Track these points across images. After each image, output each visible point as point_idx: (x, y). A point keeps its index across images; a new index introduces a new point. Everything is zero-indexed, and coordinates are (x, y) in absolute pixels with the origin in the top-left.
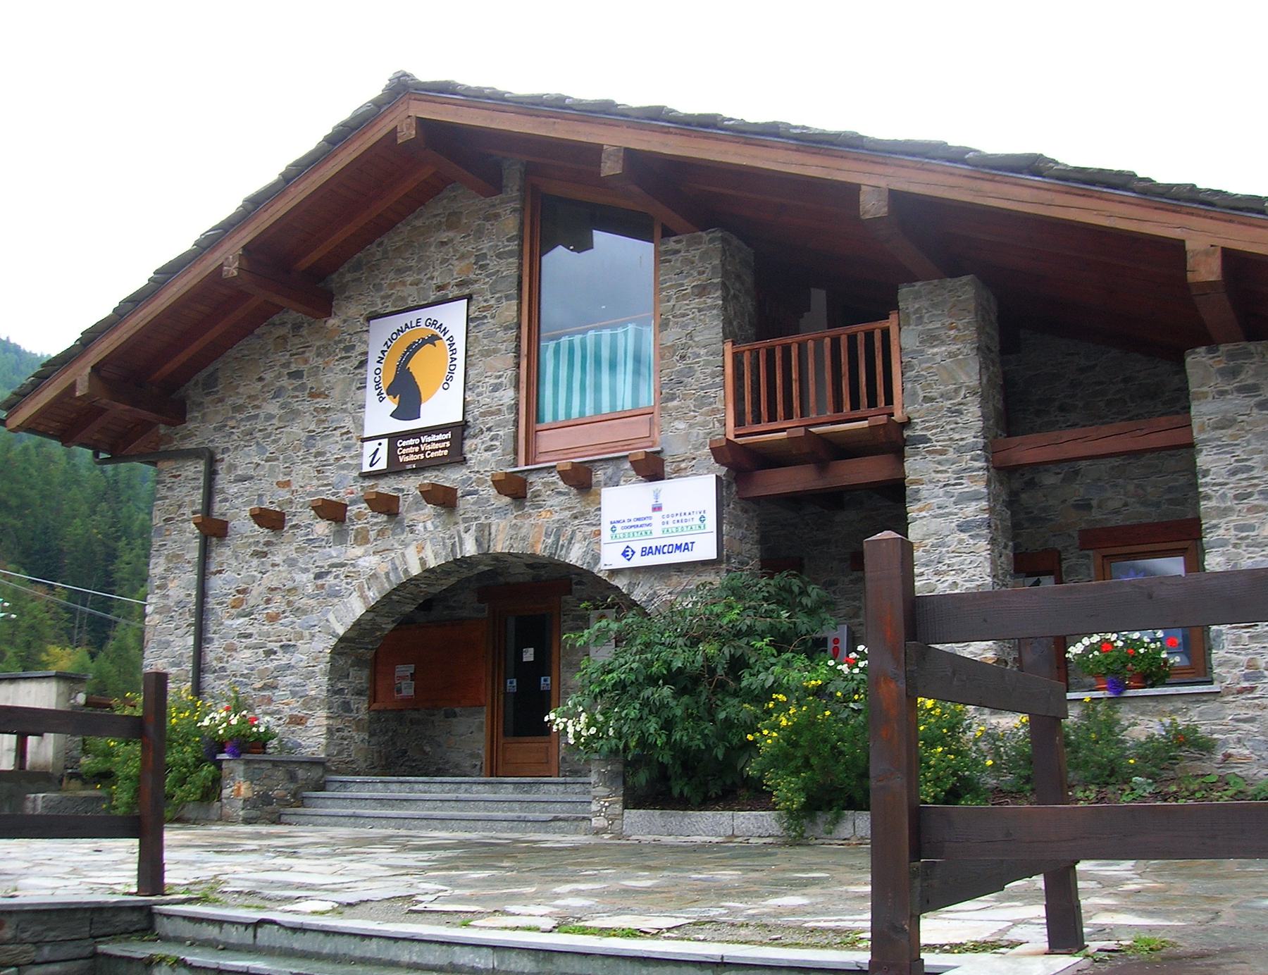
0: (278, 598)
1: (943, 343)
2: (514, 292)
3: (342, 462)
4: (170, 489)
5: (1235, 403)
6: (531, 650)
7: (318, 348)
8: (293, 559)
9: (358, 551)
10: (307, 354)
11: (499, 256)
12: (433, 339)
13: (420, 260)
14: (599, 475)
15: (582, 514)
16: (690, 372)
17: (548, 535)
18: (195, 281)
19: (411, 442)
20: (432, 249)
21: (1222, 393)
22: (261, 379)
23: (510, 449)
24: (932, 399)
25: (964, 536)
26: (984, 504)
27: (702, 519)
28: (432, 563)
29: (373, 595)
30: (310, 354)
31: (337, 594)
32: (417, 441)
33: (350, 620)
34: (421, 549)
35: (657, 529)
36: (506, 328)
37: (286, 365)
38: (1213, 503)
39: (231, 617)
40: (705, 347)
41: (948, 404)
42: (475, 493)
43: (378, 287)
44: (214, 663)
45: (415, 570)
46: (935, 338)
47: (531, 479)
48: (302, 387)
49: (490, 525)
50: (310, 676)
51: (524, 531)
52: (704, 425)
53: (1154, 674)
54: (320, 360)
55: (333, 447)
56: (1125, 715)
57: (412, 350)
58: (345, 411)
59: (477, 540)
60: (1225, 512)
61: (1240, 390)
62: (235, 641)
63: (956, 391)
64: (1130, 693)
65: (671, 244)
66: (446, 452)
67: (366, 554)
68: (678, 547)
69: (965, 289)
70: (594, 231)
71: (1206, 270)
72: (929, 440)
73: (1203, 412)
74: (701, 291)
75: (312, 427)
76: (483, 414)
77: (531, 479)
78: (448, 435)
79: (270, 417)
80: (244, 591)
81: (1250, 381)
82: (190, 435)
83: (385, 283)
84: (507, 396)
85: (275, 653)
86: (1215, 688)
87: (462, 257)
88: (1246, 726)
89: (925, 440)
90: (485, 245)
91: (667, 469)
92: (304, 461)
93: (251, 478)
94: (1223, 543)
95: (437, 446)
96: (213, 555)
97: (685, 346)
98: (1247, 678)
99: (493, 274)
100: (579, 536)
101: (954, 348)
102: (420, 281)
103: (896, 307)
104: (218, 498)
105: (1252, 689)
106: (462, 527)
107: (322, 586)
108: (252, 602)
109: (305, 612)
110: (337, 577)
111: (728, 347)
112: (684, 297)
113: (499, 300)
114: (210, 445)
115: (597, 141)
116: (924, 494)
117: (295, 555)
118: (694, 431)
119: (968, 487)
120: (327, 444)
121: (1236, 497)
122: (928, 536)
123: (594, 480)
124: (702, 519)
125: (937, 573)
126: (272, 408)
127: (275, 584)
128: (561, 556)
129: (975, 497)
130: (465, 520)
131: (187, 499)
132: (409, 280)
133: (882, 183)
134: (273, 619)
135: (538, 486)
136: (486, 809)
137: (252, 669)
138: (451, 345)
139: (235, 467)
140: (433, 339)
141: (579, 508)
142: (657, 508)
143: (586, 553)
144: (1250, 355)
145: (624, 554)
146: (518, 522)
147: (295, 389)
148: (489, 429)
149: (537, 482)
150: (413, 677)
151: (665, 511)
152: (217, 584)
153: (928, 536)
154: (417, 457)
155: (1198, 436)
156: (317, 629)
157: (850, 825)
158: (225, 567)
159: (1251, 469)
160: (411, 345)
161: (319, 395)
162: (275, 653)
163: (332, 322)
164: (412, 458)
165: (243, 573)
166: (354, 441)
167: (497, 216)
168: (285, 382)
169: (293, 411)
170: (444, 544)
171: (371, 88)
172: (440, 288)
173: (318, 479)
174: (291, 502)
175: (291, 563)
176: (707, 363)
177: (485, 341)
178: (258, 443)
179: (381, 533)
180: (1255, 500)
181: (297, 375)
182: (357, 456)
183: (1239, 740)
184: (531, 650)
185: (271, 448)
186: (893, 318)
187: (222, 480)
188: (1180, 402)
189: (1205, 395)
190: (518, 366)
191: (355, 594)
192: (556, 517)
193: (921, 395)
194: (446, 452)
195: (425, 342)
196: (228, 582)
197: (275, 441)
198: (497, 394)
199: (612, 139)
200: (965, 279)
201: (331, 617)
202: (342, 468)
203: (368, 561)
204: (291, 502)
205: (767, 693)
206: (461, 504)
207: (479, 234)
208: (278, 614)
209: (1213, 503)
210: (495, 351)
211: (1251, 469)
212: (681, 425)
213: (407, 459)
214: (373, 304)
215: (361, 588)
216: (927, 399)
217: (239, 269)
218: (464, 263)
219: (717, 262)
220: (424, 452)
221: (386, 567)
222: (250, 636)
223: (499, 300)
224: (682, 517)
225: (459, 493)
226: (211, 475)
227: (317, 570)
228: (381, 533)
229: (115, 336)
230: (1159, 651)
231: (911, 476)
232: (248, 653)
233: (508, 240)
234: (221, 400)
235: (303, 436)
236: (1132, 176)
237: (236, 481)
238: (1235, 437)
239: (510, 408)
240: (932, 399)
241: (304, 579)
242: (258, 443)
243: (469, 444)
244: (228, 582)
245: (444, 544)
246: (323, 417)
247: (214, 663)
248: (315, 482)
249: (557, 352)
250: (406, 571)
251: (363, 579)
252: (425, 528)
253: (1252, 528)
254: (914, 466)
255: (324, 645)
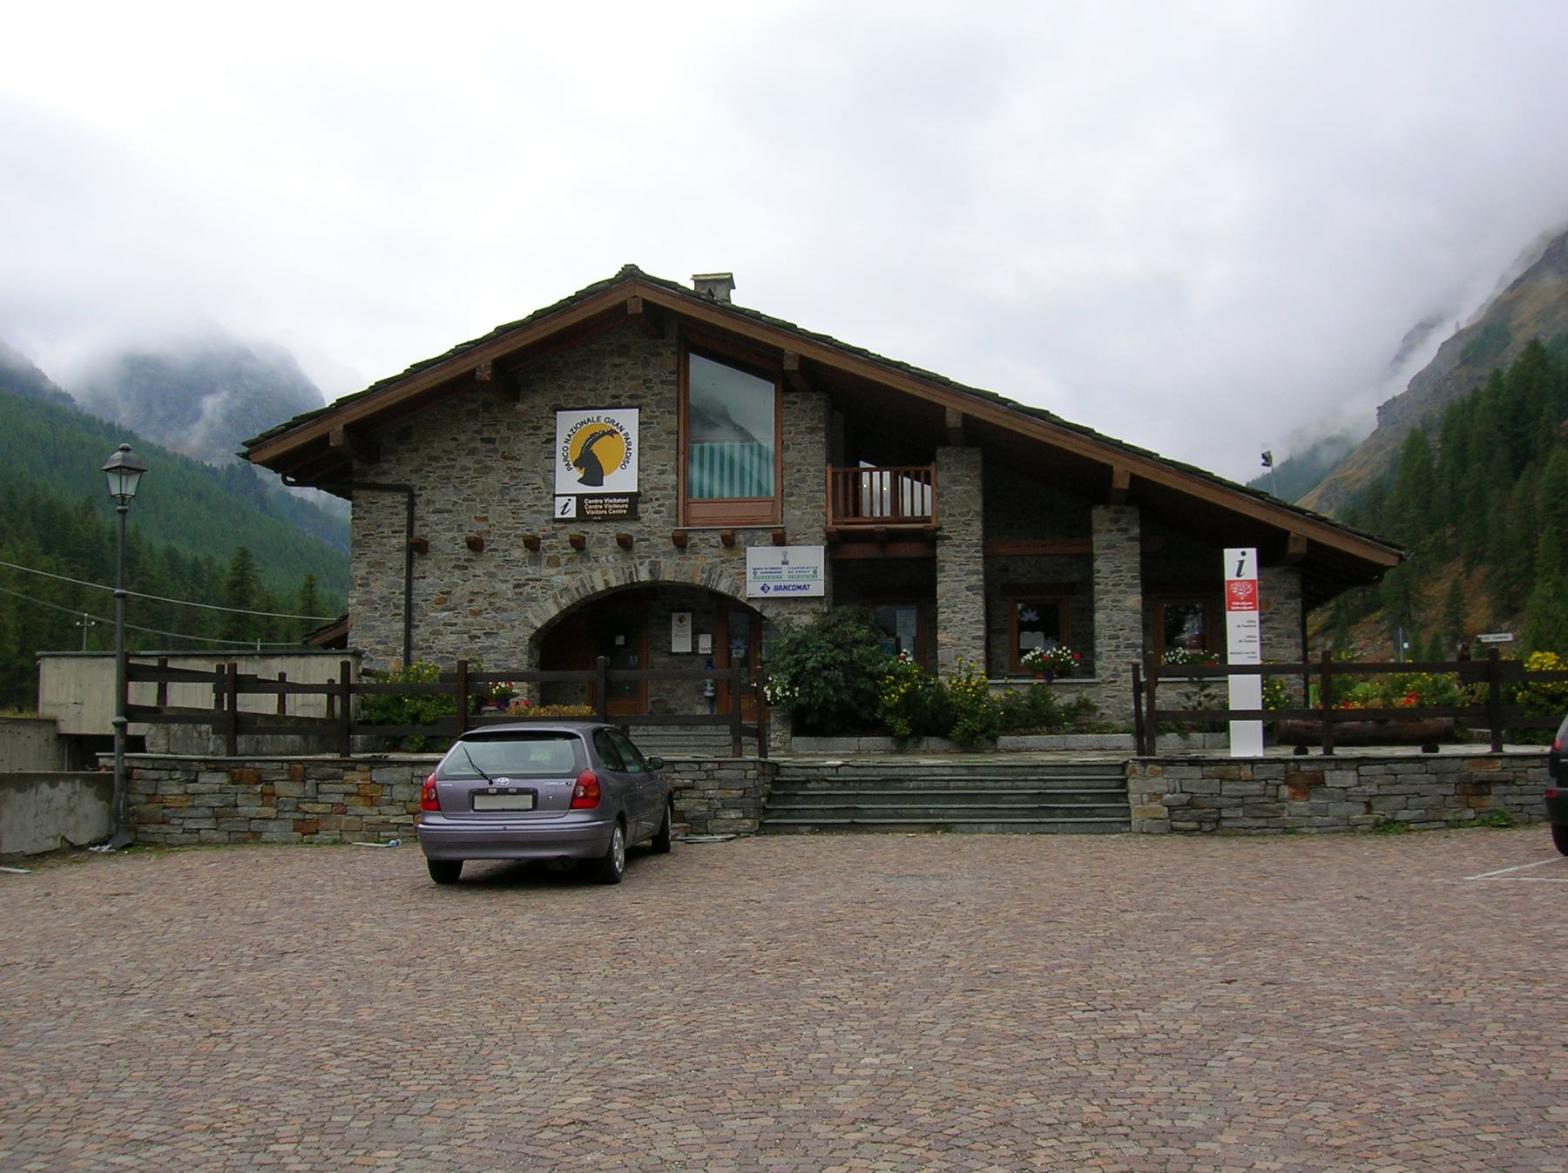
0: (480, 599)
1: (961, 484)
2: (675, 409)
3: (535, 508)
4: (366, 512)
5: (1116, 537)
6: (622, 638)
7: (509, 424)
8: (493, 573)
9: (552, 571)
10: (498, 427)
11: (663, 382)
12: (612, 433)
13: (597, 373)
14: (740, 537)
15: (728, 561)
16: (803, 480)
17: (703, 572)
18: (448, 378)
19: (596, 501)
20: (607, 367)
21: (1110, 531)
22: (455, 439)
23: (674, 514)
24: (954, 516)
25: (969, 593)
26: (981, 577)
27: (815, 572)
28: (614, 584)
29: (565, 602)
30: (502, 427)
31: (534, 600)
32: (601, 501)
33: (547, 618)
34: (604, 574)
35: (785, 575)
36: (669, 433)
37: (479, 432)
38: (1101, 587)
39: (436, 610)
40: (813, 466)
41: (963, 519)
42: (648, 540)
43: (561, 388)
44: (421, 643)
45: (600, 587)
46: (958, 481)
47: (690, 535)
48: (495, 450)
49: (659, 562)
50: (513, 654)
51: (685, 568)
52: (813, 514)
53: (1065, 671)
54: (511, 434)
55: (527, 498)
56: (1051, 690)
57: (595, 437)
58: (536, 472)
59: (650, 572)
60: (1108, 592)
61: (1118, 530)
62: (441, 628)
63: (968, 512)
64: (1055, 681)
65: (791, 397)
66: (625, 511)
67: (559, 573)
68: (799, 587)
69: (976, 456)
70: (691, 355)
71: (1122, 483)
72: (951, 538)
73: (1099, 540)
74: (812, 430)
75: (506, 480)
76: (651, 489)
77: (690, 535)
78: (627, 500)
79: (465, 469)
80: (448, 593)
81: (1124, 526)
82: (385, 473)
83: (567, 386)
84: (671, 479)
85: (479, 638)
86: (1097, 680)
87: (632, 378)
88: (1111, 700)
89: (949, 538)
90: (651, 373)
91: (788, 539)
92: (500, 504)
93: (451, 511)
94: (1105, 608)
95: (621, 506)
96: (416, 564)
97: (800, 464)
98: (1113, 676)
99: (658, 394)
100: (725, 573)
101: (968, 488)
102: (597, 389)
103: (935, 460)
104: (417, 523)
105: (1115, 682)
106: (637, 562)
107: (521, 594)
108: (455, 601)
109: (505, 610)
110: (533, 587)
111: (829, 468)
112: (801, 433)
113: (663, 413)
114: (407, 483)
115: (781, 346)
116: (946, 568)
117: (494, 570)
118: (807, 517)
119: (972, 567)
120: (519, 494)
121: (1113, 585)
122: (949, 591)
123: (737, 540)
124: (815, 572)
125: (953, 612)
126: (469, 462)
127: (476, 590)
128: (712, 585)
129: (976, 572)
130: (639, 557)
131: (386, 521)
132: (588, 387)
133: (959, 408)
134: (476, 613)
135: (696, 540)
136: (669, 740)
137: (458, 648)
138: (627, 439)
139: (434, 502)
140: (612, 433)
141: (727, 557)
142: (785, 563)
143: (731, 585)
144: (1125, 513)
145: (762, 588)
146: (681, 562)
147: (489, 451)
148: (657, 499)
149: (695, 538)
150: (1458, 678)
151: (790, 565)
152: (420, 586)
153: (949, 591)
154: (601, 512)
155: (1095, 551)
156: (517, 622)
157: (925, 744)
158: (428, 574)
159: (1121, 571)
160: (593, 435)
161: (512, 458)
162: (479, 638)
163: (520, 407)
164: (598, 512)
165: (445, 580)
166: (544, 494)
167: (660, 354)
168: (478, 444)
169: (486, 467)
170: (624, 573)
171: (610, 272)
172: (614, 397)
173: (514, 518)
174: (489, 532)
175: (491, 575)
176: (816, 477)
177: (652, 440)
178: (455, 486)
179: (570, 560)
180: (1122, 587)
181: (491, 441)
182: (548, 505)
183: (1108, 707)
184: (622, 638)
185: (469, 492)
186: (933, 464)
187: (420, 510)
188: (1087, 531)
189: (1100, 531)
190: (678, 460)
191: (550, 601)
192: (709, 561)
193: (948, 512)
194: (625, 511)
195: (604, 434)
196: (431, 586)
197: (471, 487)
198: (663, 476)
199: (790, 347)
200: (975, 449)
201: (530, 615)
202: (535, 512)
203: (560, 578)
204: (489, 532)
205: (881, 676)
206: (636, 546)
207: (646, 364)
208: (481, 611)
209: (1101, 587)
210: (661, 448)
211: (1121, 571)
212: (798, 513)
213: (593, 513)
214: (556, 399)
215: (554, 596)
216: (950, 515)
217: (491, 375)
218: (634, 383)
219: (821, 414)
220: (607, 509)
221: (574, 584)
222: (455, 624)
223: (663, 413)
224: (802, 569)
225: (635, 539)
226: (411, 506)
227: (516, 582)
228: (570, 560)
229: (368, 405)
230: (1070, 660)
231: (940, 558)
232: (454, 637)
233: (670, 373)
234: (417, 450)
235: (499, 486)
236: (1092, 430)
237: (433, 512)
238: (1114, 554)
239: (673, 487)
240: (954, 516)
241: (507, 588)
242: (455, 486)
243: (641, 507)
244: (431, 586)
245: (624, 573)
246: (515, 474)
247: (421, 643)
248: (510, 520)
249: (702, 450)
250: (593, 588)
251: (556, 591)
252: (607, 560)
253: (1120, 601)
254: (942, 552)
255: (526, 634)
